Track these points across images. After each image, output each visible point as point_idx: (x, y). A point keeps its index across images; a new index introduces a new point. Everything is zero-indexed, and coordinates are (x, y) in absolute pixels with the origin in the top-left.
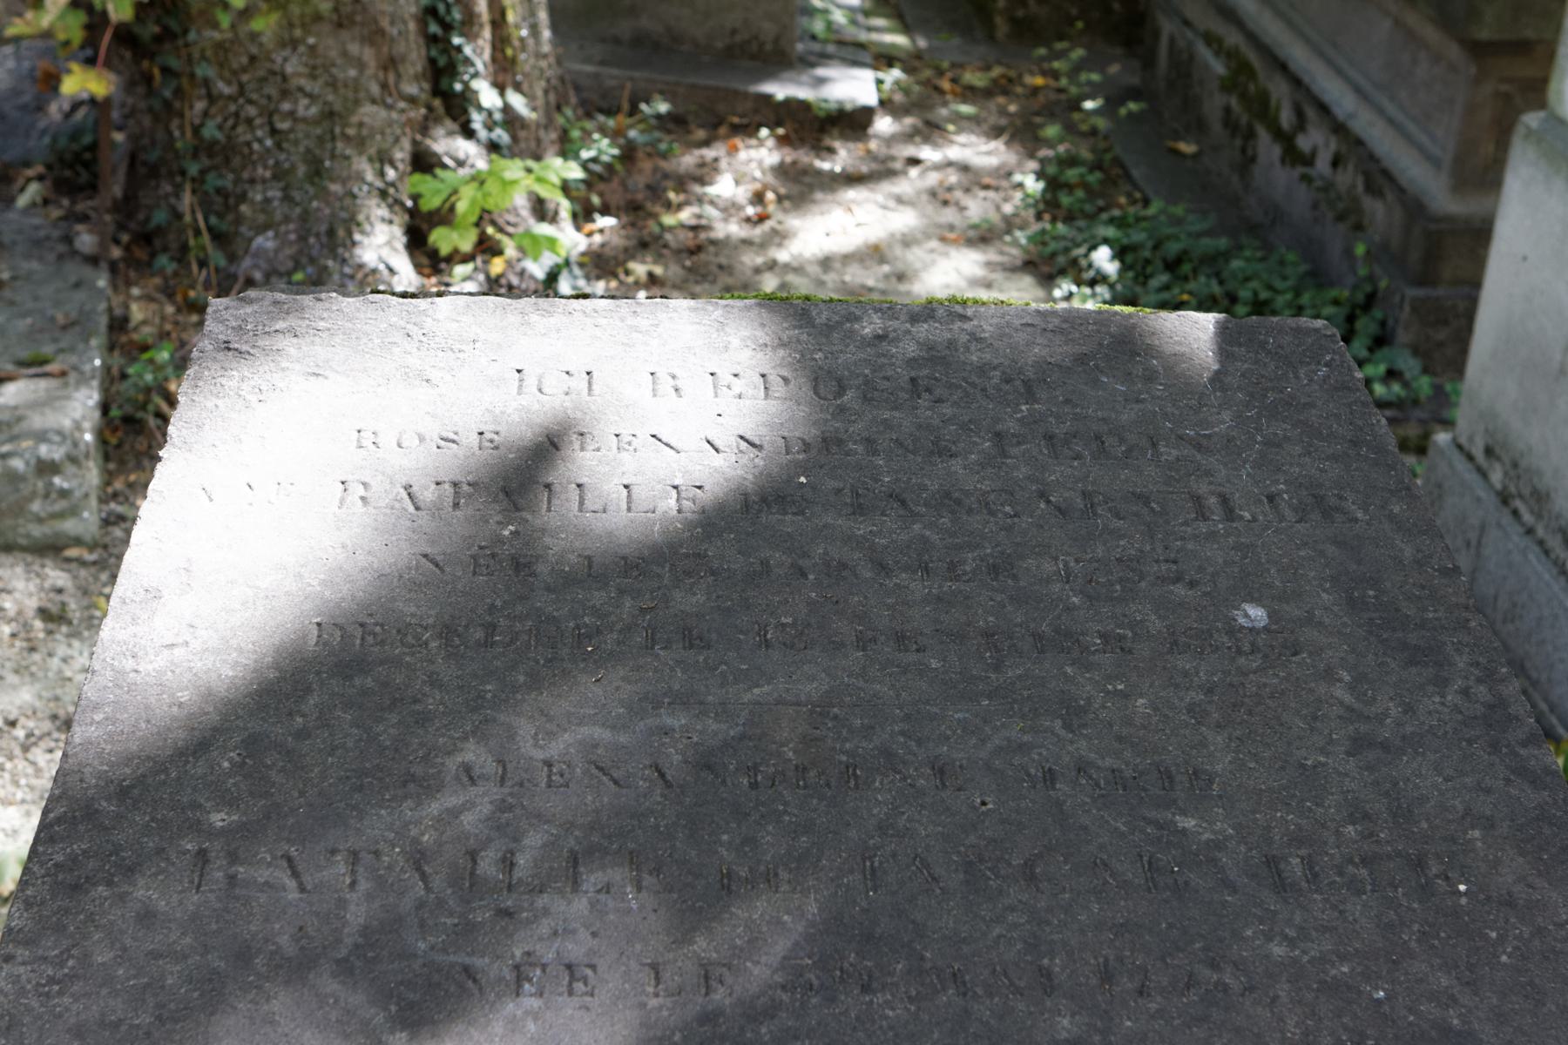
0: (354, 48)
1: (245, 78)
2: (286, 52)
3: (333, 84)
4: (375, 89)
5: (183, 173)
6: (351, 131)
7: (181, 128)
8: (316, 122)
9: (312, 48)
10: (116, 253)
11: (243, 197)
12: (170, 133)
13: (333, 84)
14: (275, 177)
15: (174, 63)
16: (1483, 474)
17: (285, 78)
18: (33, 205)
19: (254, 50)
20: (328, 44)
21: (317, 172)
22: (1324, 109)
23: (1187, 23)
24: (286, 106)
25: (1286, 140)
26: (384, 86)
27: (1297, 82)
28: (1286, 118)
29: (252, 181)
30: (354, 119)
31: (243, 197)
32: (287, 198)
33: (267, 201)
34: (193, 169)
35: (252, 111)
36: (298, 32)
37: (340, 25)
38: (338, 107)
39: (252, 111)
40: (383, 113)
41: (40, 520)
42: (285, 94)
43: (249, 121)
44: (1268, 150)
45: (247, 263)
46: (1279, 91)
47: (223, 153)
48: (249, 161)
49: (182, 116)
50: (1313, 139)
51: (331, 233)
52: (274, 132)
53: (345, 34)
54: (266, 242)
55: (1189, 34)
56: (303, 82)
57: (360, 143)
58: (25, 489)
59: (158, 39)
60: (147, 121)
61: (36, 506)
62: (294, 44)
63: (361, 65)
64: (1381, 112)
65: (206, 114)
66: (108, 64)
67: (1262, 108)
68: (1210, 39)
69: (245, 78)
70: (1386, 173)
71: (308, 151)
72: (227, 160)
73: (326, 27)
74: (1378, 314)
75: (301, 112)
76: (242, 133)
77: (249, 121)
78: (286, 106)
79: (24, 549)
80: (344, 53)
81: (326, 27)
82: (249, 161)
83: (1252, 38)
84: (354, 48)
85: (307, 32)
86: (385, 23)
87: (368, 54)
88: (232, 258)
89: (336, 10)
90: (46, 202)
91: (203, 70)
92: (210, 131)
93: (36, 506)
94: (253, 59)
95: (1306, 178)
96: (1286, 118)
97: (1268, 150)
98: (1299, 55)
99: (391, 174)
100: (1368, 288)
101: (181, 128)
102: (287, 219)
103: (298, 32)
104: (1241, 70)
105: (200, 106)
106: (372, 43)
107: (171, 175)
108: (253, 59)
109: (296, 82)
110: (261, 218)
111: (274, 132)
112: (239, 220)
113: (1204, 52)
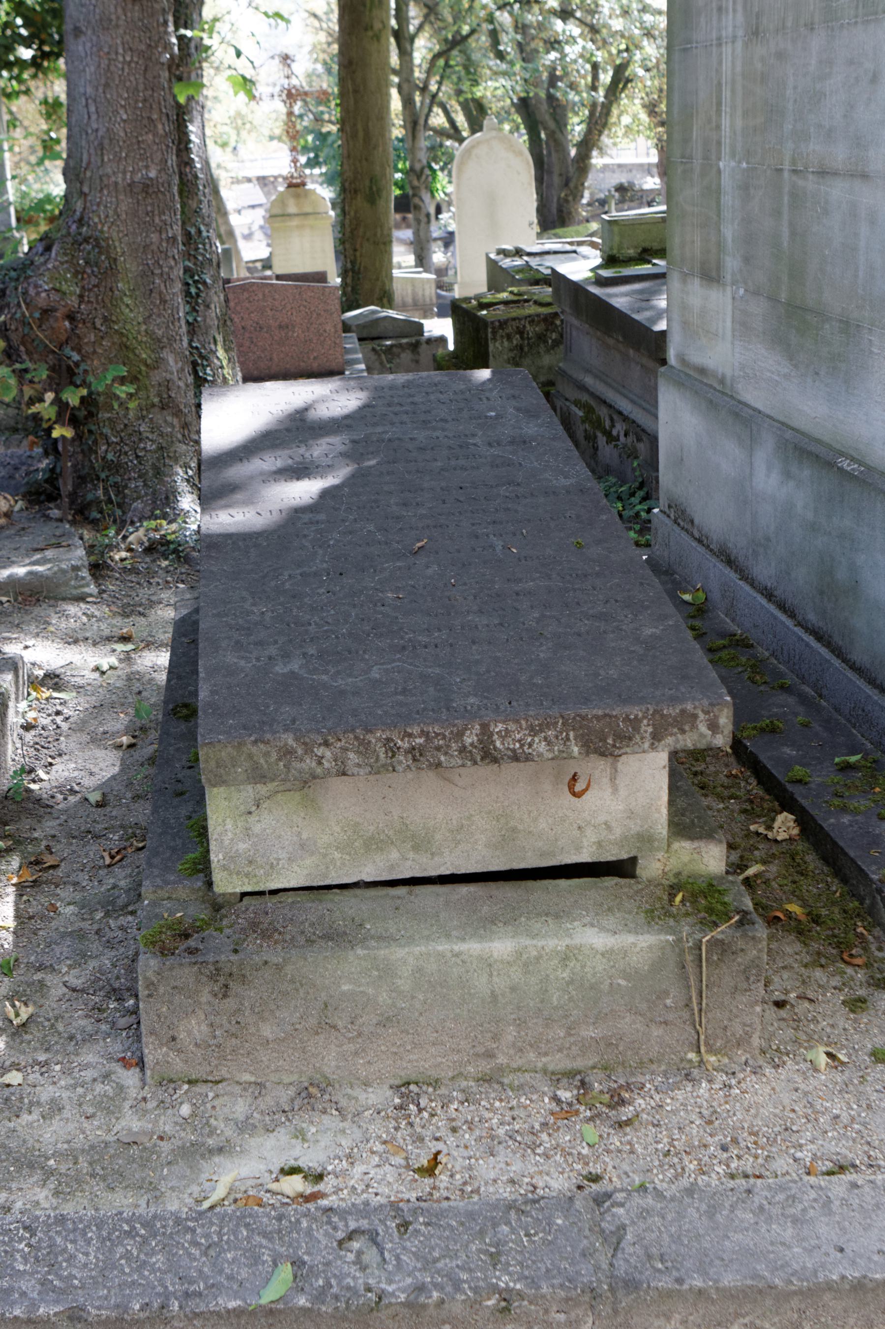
0: (169, 419)
1: (123, 434)
2: (140, 422)
3: (161, 435)
4: (180, 436)
5: (98, 478)
6: (171, 455)
7: (96, 458)
8: (156, 452)
9: (151, 419)
10: (70, 518)
11: (126, 487)
12: (91, 461)
13: (161, 435)
14: (140, 477)
15: (93, 428)
16: (669, 516)
17: (140, 434)
18: (22, 510)
19: (126, 422)
20: (156, 416)
21: (158, 473)
22: (620, 413)
23: (567, 399)
24: (142, 445)
25: (608, 434)
26: (184, 436)
27: (610, 406)
28: (607, 424)
29: (130, 479)
30: (172, 449)
31: (126, 487)
32: (145, 485)
33: (136, 487)
34: (103, 476)
35: (126, 448)
36: (145, 413)
37: (163, 409)
38: (164, 445)
39: (126, 448)
40: (184, 447)
41: (75, 588)
42: (141, 440)
43: (126, 453)
44: (602, 440)
45: (130, 514)
46: (603, 412)
47: (115, 467)
48: (126, 470)
49: (96, 453)
50: (619, 428)
51: (167, 498)
52: (137, 457)
53: (165, 412)
54: (138, 505)
55: (568, 403)
56: (148, 434)
57: (176, 460)
58: (69, 576)
59: (86, 418)
60: (80, 457)
61: (73, 583)
62: (143, 418)
63: (173, 427)
64: (640, 406)
65: (106, 451)
66: (69, 424)
67: (598, 424)
68: (577, 403)
69: (123, 434)
70: (643, 430)
71: (153, 464)
72: (117, 471)
73: (156, 410)
74: (645, 489)
75: (148, 448)
76: (124, 459)
77: (126, 453)
78: (142, 445)
79: (70, 599)
80: (166, 421)
81: (156, 410)
82: (126, 470)
83: (592, 395)
84: (169, 419)
85: (148, 412)
86: (182, 407)
87: (175, 421)
88: (124, 513)
89: (161, 401)
90: (27, 509)
91: (106, 431)
92: (110, 456)
93: (73, 583)
94: (126, 425)
95: (616, 446)
96: (607, 424)
97: (602, 440)
98: (610, 395)
99: (190, 473)
100: (640, 480)
101: (96, 458)
102: (146, 494)
103: (145, 413)
104: (589, 410)
105: (104, 448)
106: (177, 416)
107: (92, 481)
108: (126, 425)
109: (145, 435)
110: (135, 495)
111: (137, 457)
112: (125, 497)
113: (574, 409)
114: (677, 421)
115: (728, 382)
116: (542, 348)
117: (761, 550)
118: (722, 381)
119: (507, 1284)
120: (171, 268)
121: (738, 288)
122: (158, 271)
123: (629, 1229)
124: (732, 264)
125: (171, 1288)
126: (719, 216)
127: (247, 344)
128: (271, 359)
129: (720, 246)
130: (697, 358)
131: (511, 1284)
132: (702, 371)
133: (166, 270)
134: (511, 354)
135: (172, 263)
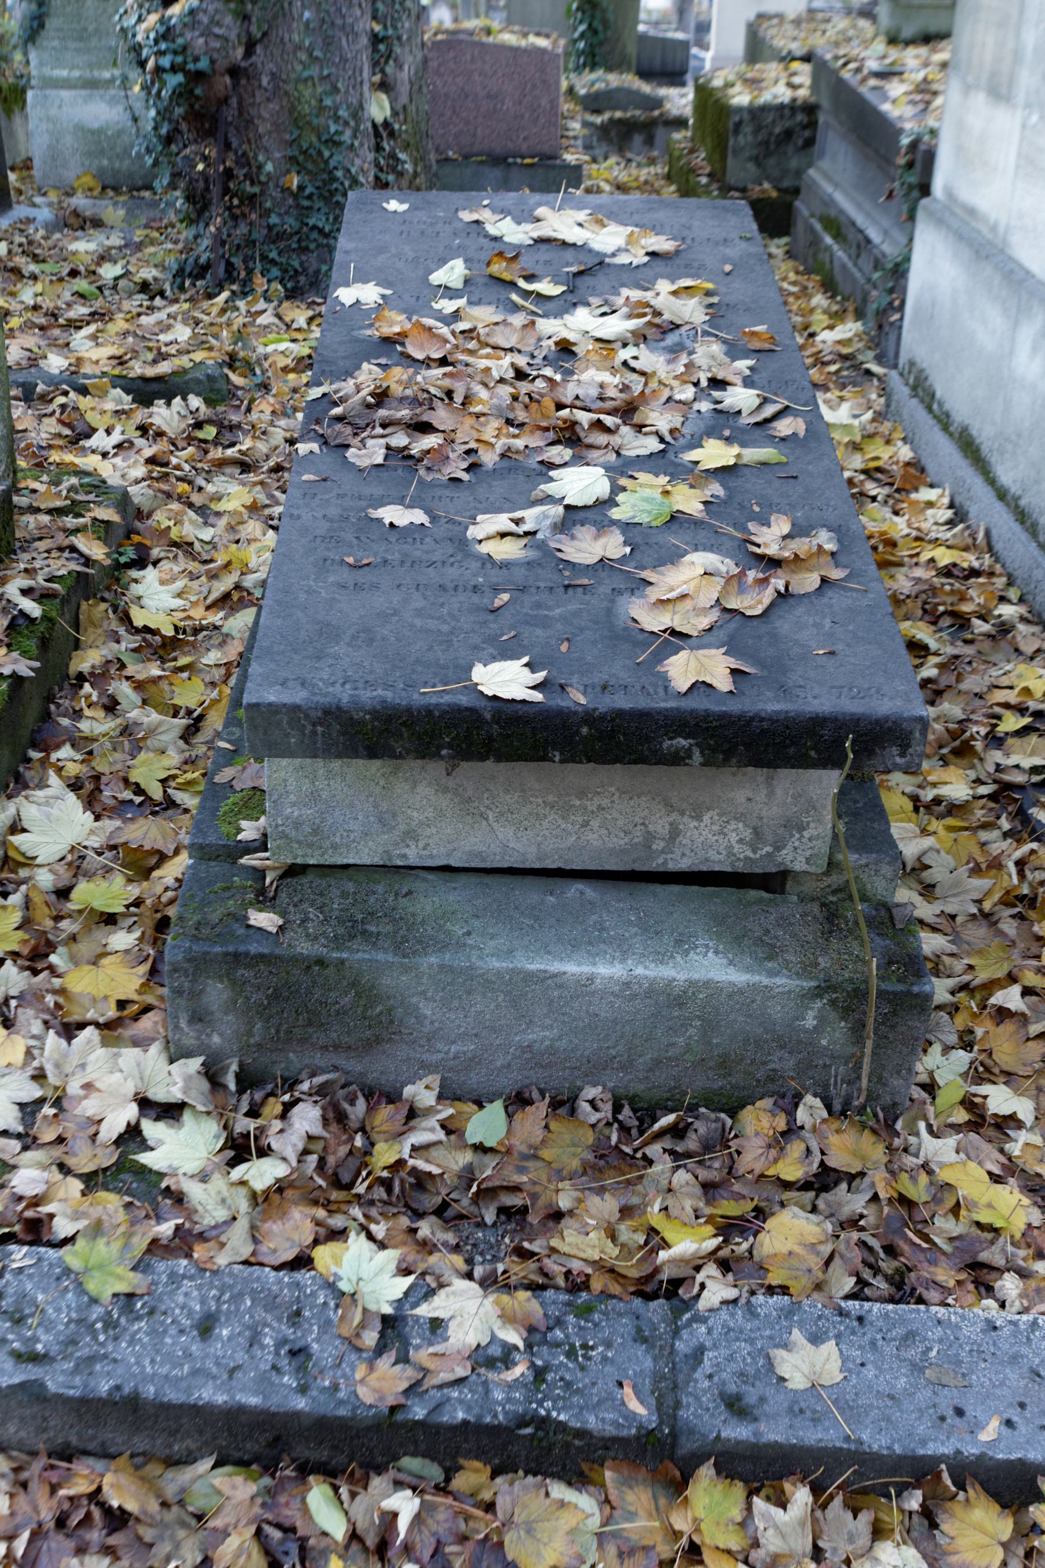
114: (934, 266)
115: (1001, 230)
116: (790, 149)
117: (1009, 447)
118: (994, 229)
119: (548, 1411)
120: (356, 19)
121: (1030, 114)
122: (339, 22)
123: (709, 1355)
124: (1026, 80)
125: (148, 1369)
126: (1021, 12)
127: (449, 113)
128: (474, 135)
129: (1017, 56)
130: (966, 195)
131: (554, 1414)
132: (972, 212)
133: (349, 20)
134: (755, 152)
135: (358, 13)
